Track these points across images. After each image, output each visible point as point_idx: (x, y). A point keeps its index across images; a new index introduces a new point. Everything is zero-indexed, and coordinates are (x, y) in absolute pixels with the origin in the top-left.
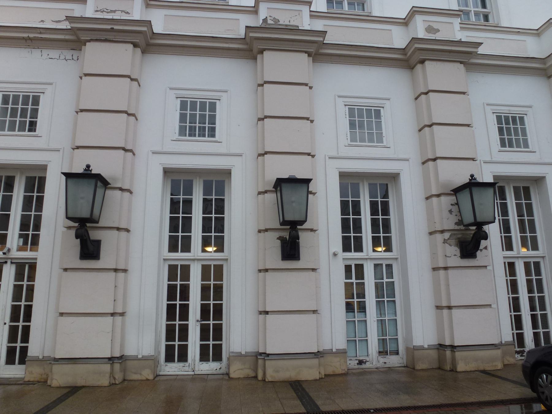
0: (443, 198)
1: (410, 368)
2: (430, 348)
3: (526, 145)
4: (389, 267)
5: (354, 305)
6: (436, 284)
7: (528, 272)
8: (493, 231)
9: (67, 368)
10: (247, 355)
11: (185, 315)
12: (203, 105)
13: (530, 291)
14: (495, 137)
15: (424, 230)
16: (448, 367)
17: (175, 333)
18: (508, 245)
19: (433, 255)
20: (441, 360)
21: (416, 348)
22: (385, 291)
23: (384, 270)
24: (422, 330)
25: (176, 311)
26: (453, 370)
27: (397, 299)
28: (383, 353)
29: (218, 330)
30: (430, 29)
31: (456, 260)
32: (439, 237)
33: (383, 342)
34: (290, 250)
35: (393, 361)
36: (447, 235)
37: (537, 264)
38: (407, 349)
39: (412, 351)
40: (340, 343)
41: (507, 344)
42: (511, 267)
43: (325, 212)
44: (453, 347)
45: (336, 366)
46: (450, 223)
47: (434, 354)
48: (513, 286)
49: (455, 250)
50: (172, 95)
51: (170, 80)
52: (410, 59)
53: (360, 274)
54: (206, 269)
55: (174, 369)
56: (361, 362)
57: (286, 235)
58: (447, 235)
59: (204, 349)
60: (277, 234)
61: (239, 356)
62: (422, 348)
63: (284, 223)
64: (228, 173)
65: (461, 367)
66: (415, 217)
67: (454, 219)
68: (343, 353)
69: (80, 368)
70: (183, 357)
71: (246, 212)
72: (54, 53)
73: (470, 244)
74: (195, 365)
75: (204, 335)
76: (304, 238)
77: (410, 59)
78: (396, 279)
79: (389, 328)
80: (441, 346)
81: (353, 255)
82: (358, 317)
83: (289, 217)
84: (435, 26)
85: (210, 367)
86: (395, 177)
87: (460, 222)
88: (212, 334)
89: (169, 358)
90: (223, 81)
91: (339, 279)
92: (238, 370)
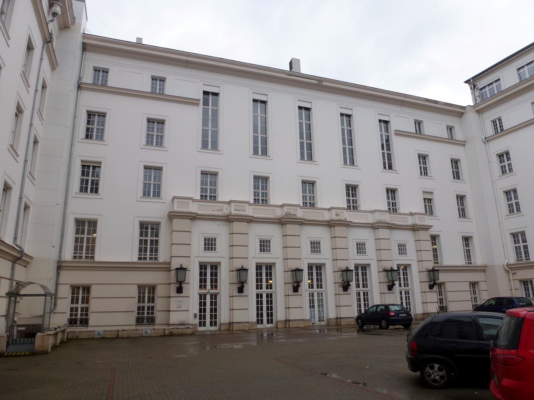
0: (289, 272)
1: (328, 325)
2: (334, 319)
3: (365, 253)
4: (322, 293)
5: (312, 306)
6: (336, 299)
7: (364, 295)
8: (397, 283)
9: (238, 325)
10: (283, 321)
11: (262, 310)
12: (266, 241)
13: (406, 300)
14: (398, 251)
15: (283, 283)
16: (339, 324)
17: (259, 315)
18: (358, 286)
19: (335, 290)
20: (337, 322)
21: (330, 319)
22: (320, 301)
23: (320, 294)
24: (331, 313)
25: (259, 309)
26: (340, 325)
27: (324, 304)
28: (320, 321)
29: (216, 316)
30: (337, 215)
31: (292, 293)
32: (337, 284)
33: (319, 317)
34: (241, 290)
35: (323, 323)
36: (339, 284)
37: (408, 291)
38: (414, 315)
39: (329, 320)
40: (308, 317)
41: (254, 323)
42: (359, 294)
43: (193, 277)
44: (340, 318)
45: (307, 324)
46: (340, 281)
47: (335, 320)
48: (359, 300)
49: (342, 289)
50: (257, 237)
51: (204, 229)
52: (281, 222)
53: (313, 296)
54: (267, 295)
55: (259, 326)
56: (313, 324)
57: (295, 285)
58: (339, 284)
59: (211, 322)
60: (291, 285)
61: (224, 324)
62: (331, 319)
63: (177, 281)
64: (220, 263)
65: (342, 324)
66: (330, 278)
67: (342, 279)
68: (309, 320)
69: (240, 325)
70: (204, 325)
71: (225, 277)
72: (219, 223)
73: (346, 287)
74: (208, 327)
75: (268, 316)
76: (184, 285)
77: (281, 222)
78: (323, 297)
79: (321, 313)
80: (337, 318)
81: (259, 290)
82: (312, 309)
83: (179, 280)
84: (339, 213)
85: (213, 328)
86: (369, 265)
87: (343, 280)
88: (214, 317)
89: (200, 326)
90: (272, 233)
91: (307, 298)
92: (223, 328)
